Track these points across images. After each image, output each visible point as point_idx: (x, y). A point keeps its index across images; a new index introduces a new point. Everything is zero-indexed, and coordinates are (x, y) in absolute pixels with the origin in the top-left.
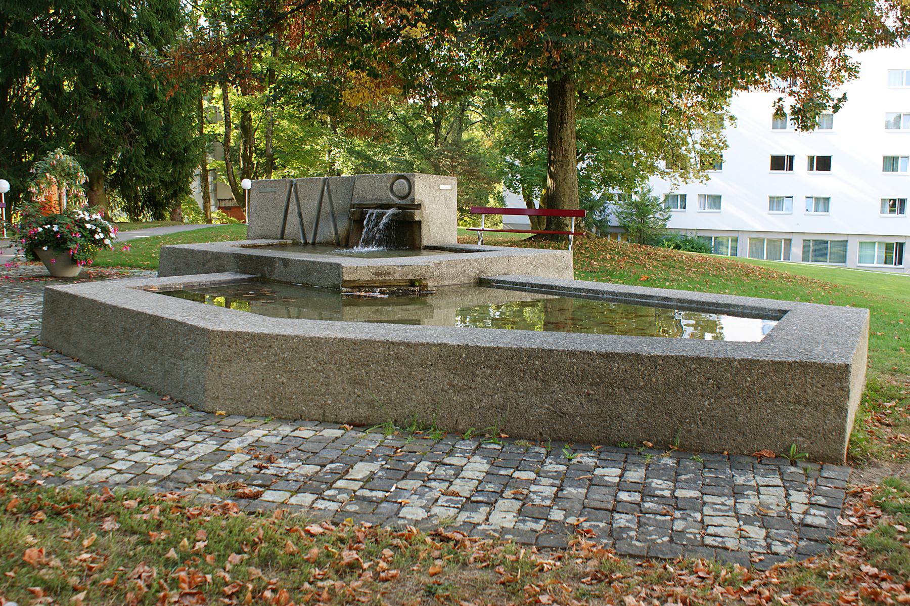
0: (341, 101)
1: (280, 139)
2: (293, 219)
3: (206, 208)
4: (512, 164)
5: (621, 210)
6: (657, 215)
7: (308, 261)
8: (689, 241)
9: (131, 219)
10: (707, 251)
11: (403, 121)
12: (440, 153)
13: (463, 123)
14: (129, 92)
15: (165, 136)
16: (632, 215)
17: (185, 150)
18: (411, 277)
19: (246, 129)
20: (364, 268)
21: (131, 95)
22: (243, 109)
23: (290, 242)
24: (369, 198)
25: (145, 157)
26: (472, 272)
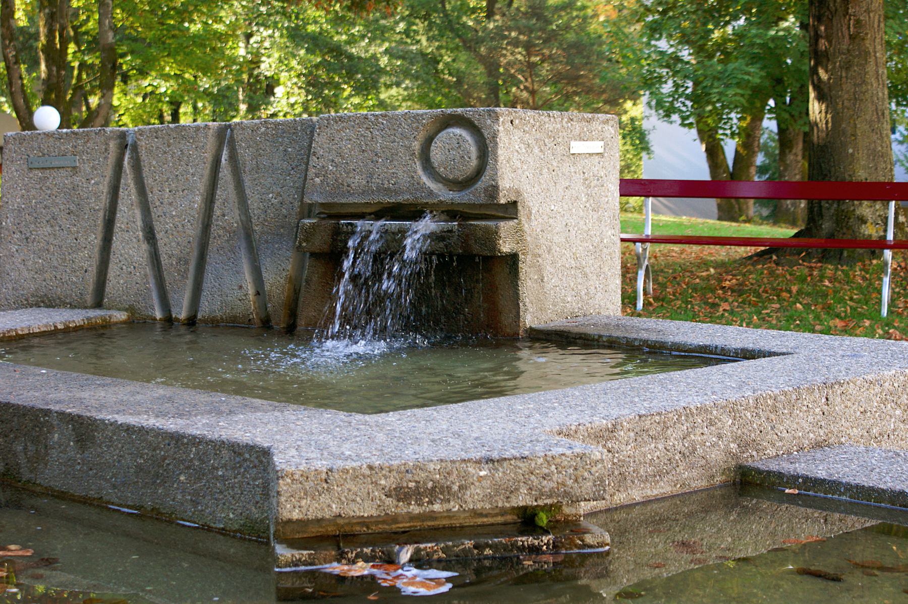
2: (129, 248)
4: (678, 60)
12: (499, 34)
18: (523, 499)
20: (356, 475)
23: (122, 316)
26: (717, 450)
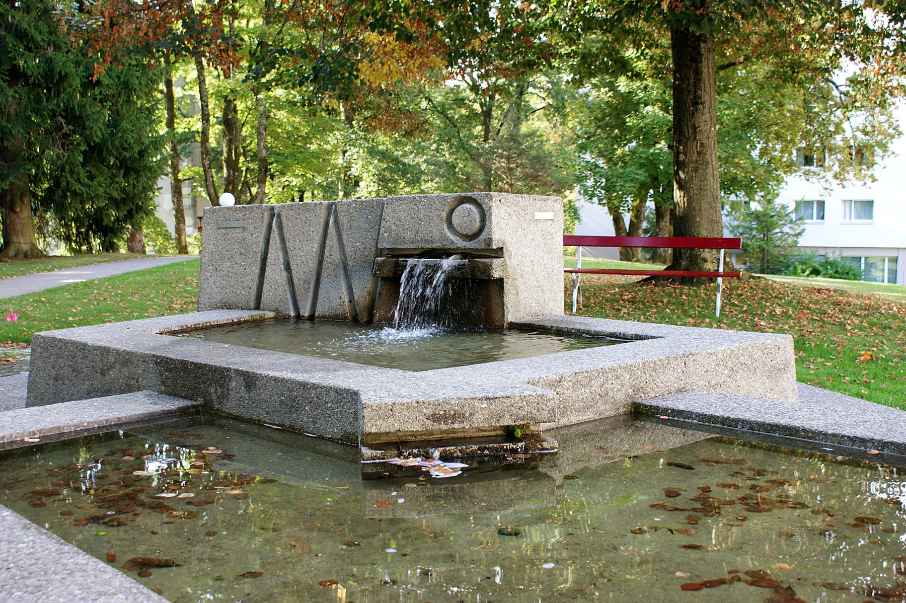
0: (357, 77)
1: (276, 137)
2: (276, 274)
3: (179, 230)
4: (597, 166)
5: (736, 223)
6: (786, 229)
7: (293, 382)
8: (831, 264)
9: (71, 250)
10: (856, 277)
11: (441, 110)
12: (491, 151)
13: (521, 111)
14: (60, 73)
15: (112, 134)
16: (751, 229)
17: (141, 153)
18: (507, 421)
19: (229, 124)
20: (409, 407)
21: (63, 78)
22: (226, 97)
23: (271, 314)
24: (409, 238)
25: (83, 165)
26: (621, 394)
